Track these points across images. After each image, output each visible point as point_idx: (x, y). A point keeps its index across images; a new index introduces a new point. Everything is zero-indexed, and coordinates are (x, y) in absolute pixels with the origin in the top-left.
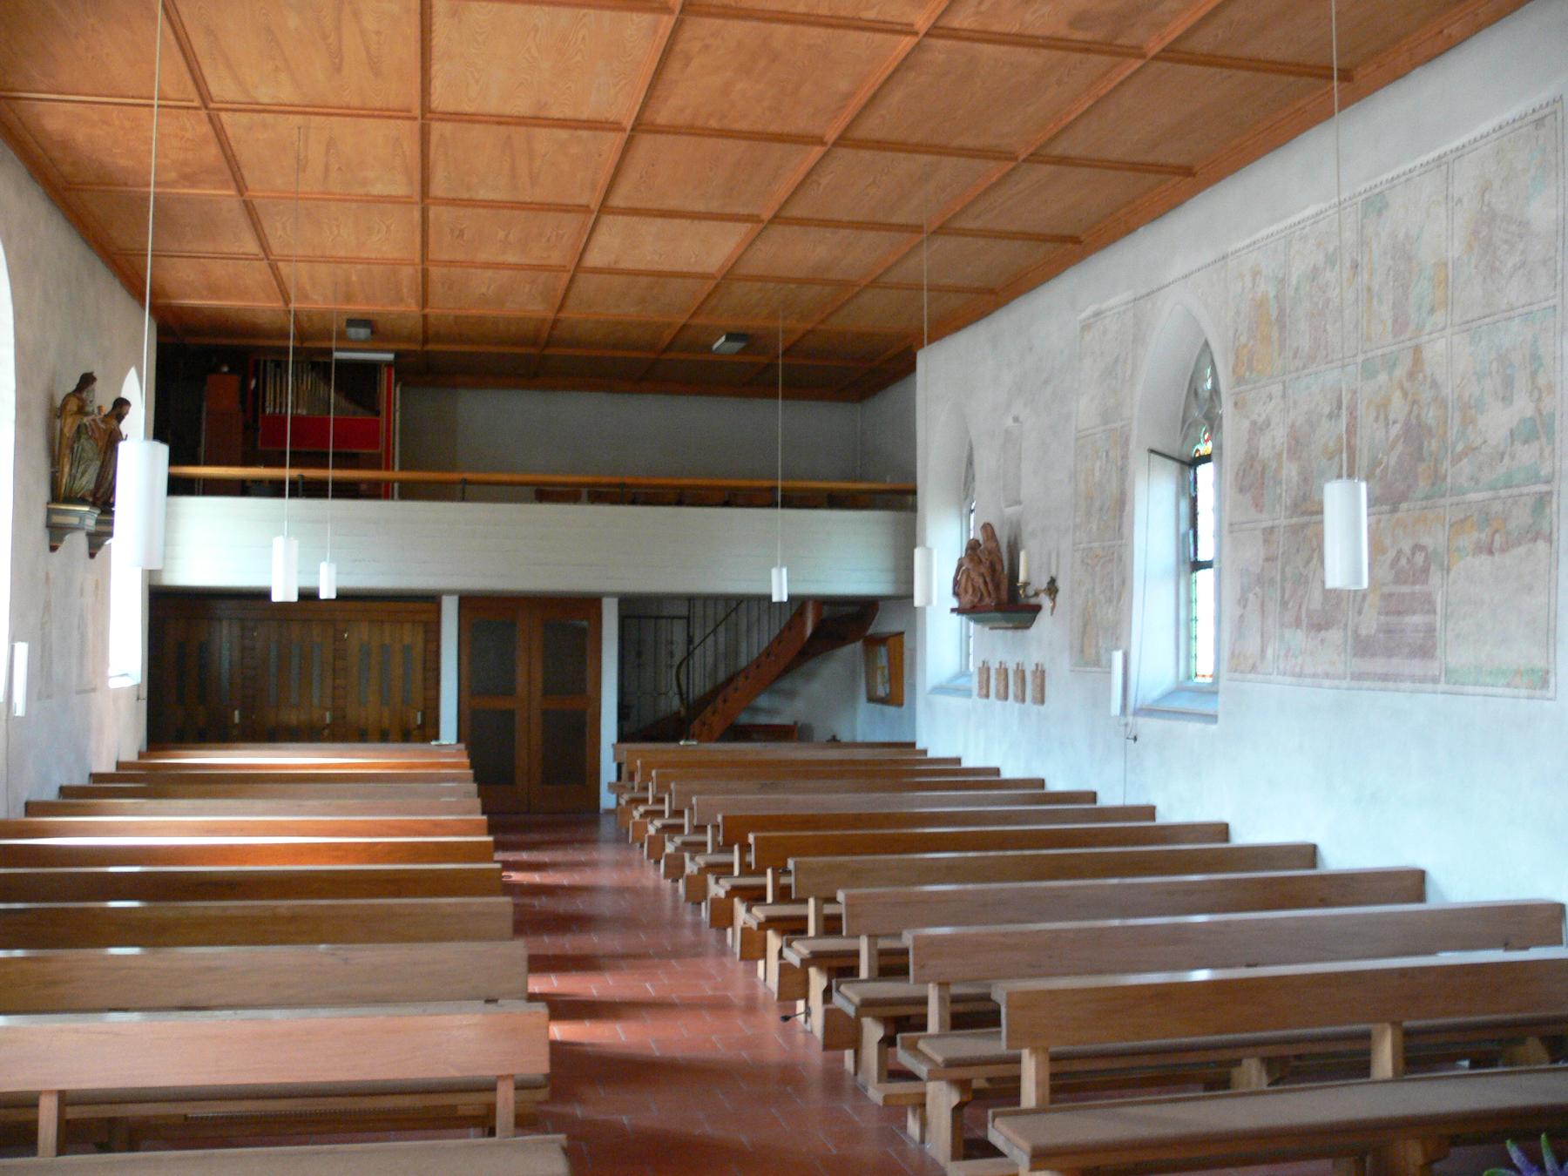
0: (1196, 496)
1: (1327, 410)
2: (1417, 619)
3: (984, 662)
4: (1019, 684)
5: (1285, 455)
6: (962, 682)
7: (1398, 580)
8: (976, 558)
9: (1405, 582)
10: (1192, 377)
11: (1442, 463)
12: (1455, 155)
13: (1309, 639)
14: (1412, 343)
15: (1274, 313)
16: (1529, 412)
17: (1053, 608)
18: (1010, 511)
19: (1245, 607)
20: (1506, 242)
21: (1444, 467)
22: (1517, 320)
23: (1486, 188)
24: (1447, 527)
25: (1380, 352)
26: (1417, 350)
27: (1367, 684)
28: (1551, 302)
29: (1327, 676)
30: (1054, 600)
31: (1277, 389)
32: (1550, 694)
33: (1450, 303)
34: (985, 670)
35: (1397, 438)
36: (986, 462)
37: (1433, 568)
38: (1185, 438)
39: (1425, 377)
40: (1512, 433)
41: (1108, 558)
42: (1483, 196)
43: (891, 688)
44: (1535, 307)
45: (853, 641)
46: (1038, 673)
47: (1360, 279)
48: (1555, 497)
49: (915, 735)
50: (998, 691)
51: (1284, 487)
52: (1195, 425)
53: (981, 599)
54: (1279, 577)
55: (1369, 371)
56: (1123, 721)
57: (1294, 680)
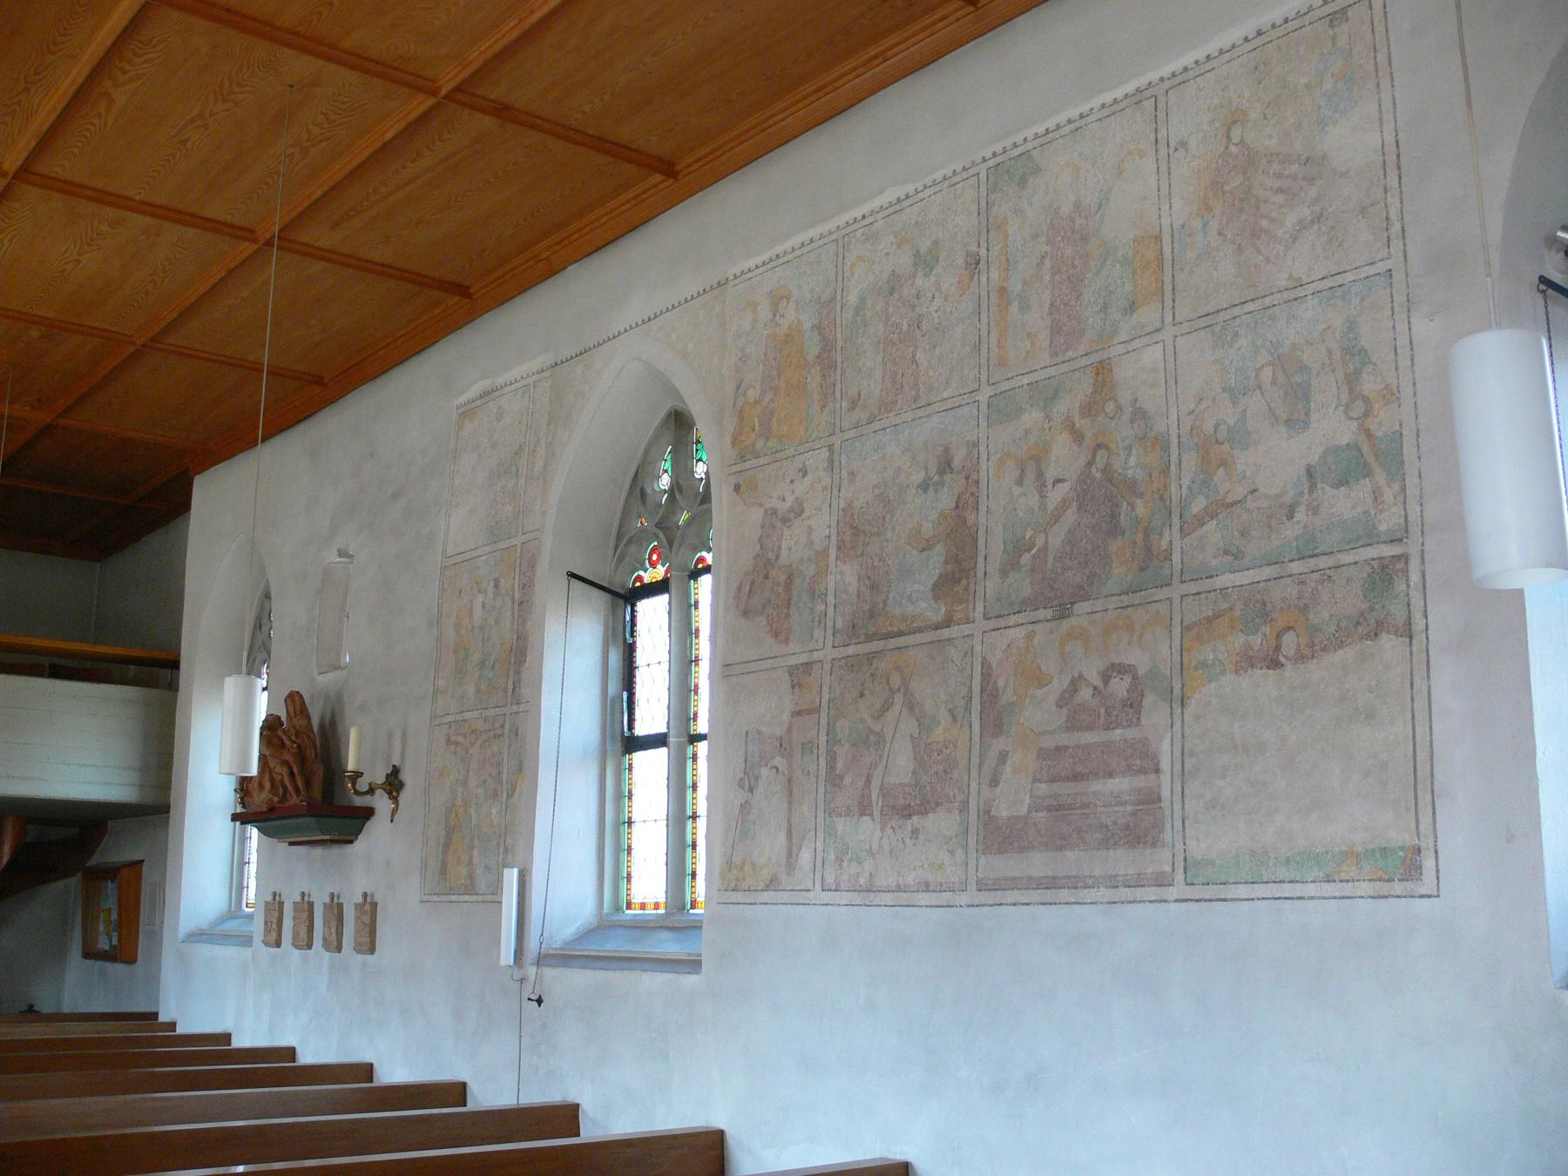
0: (634, 643)
1: (918, 477)
2: (1119, 785)
3: (275, 894)
4: (333, 923)
5: (833, 552)
6: (232, 925)
7: (1073, 725)
8: (276, 741)
9: (1090, 727)
10: (636, 475)
11: (1161, 534)
12: (1167, 84)
13: (889, 831)
14: (1095, 358)
15: (813, 348)
16: (1346, 434)
17: (394, 812)
18: (324, 680)
19: (751, 790)
20: (1280, 191)
21: (1166, 539)
22: (1312, 302)
23: (1235, 119)
24: (1177, 631)
25: (1025, 380)
26: (1103, 371)
27: (1011, 896)
28: (1381, 267)
29: (926, 887)
30: (395, 800)
31: (816, 460)
32: (1427, 884)
33: (1168, 289)
34: (274, 907)
35: (1064, 505)
36: (289, 616)
37: (1149, 699)
38: (620, 560)
39: (1119, 408)
40: (1310, 472)
41: (492, 734)
42: (1229, 129)
43: (120, 940)
44: (1350, 277)
45: (67, 875)
46: (367, 907)
47: (984, 279)
49: (156, 999)
50: (295, 937)
51: (831, 599)
52: (640, 538)
53: (284, 798)
54: (823, 738)
55: (1001, 410)
56: (518, 974)
57: (857, 898)
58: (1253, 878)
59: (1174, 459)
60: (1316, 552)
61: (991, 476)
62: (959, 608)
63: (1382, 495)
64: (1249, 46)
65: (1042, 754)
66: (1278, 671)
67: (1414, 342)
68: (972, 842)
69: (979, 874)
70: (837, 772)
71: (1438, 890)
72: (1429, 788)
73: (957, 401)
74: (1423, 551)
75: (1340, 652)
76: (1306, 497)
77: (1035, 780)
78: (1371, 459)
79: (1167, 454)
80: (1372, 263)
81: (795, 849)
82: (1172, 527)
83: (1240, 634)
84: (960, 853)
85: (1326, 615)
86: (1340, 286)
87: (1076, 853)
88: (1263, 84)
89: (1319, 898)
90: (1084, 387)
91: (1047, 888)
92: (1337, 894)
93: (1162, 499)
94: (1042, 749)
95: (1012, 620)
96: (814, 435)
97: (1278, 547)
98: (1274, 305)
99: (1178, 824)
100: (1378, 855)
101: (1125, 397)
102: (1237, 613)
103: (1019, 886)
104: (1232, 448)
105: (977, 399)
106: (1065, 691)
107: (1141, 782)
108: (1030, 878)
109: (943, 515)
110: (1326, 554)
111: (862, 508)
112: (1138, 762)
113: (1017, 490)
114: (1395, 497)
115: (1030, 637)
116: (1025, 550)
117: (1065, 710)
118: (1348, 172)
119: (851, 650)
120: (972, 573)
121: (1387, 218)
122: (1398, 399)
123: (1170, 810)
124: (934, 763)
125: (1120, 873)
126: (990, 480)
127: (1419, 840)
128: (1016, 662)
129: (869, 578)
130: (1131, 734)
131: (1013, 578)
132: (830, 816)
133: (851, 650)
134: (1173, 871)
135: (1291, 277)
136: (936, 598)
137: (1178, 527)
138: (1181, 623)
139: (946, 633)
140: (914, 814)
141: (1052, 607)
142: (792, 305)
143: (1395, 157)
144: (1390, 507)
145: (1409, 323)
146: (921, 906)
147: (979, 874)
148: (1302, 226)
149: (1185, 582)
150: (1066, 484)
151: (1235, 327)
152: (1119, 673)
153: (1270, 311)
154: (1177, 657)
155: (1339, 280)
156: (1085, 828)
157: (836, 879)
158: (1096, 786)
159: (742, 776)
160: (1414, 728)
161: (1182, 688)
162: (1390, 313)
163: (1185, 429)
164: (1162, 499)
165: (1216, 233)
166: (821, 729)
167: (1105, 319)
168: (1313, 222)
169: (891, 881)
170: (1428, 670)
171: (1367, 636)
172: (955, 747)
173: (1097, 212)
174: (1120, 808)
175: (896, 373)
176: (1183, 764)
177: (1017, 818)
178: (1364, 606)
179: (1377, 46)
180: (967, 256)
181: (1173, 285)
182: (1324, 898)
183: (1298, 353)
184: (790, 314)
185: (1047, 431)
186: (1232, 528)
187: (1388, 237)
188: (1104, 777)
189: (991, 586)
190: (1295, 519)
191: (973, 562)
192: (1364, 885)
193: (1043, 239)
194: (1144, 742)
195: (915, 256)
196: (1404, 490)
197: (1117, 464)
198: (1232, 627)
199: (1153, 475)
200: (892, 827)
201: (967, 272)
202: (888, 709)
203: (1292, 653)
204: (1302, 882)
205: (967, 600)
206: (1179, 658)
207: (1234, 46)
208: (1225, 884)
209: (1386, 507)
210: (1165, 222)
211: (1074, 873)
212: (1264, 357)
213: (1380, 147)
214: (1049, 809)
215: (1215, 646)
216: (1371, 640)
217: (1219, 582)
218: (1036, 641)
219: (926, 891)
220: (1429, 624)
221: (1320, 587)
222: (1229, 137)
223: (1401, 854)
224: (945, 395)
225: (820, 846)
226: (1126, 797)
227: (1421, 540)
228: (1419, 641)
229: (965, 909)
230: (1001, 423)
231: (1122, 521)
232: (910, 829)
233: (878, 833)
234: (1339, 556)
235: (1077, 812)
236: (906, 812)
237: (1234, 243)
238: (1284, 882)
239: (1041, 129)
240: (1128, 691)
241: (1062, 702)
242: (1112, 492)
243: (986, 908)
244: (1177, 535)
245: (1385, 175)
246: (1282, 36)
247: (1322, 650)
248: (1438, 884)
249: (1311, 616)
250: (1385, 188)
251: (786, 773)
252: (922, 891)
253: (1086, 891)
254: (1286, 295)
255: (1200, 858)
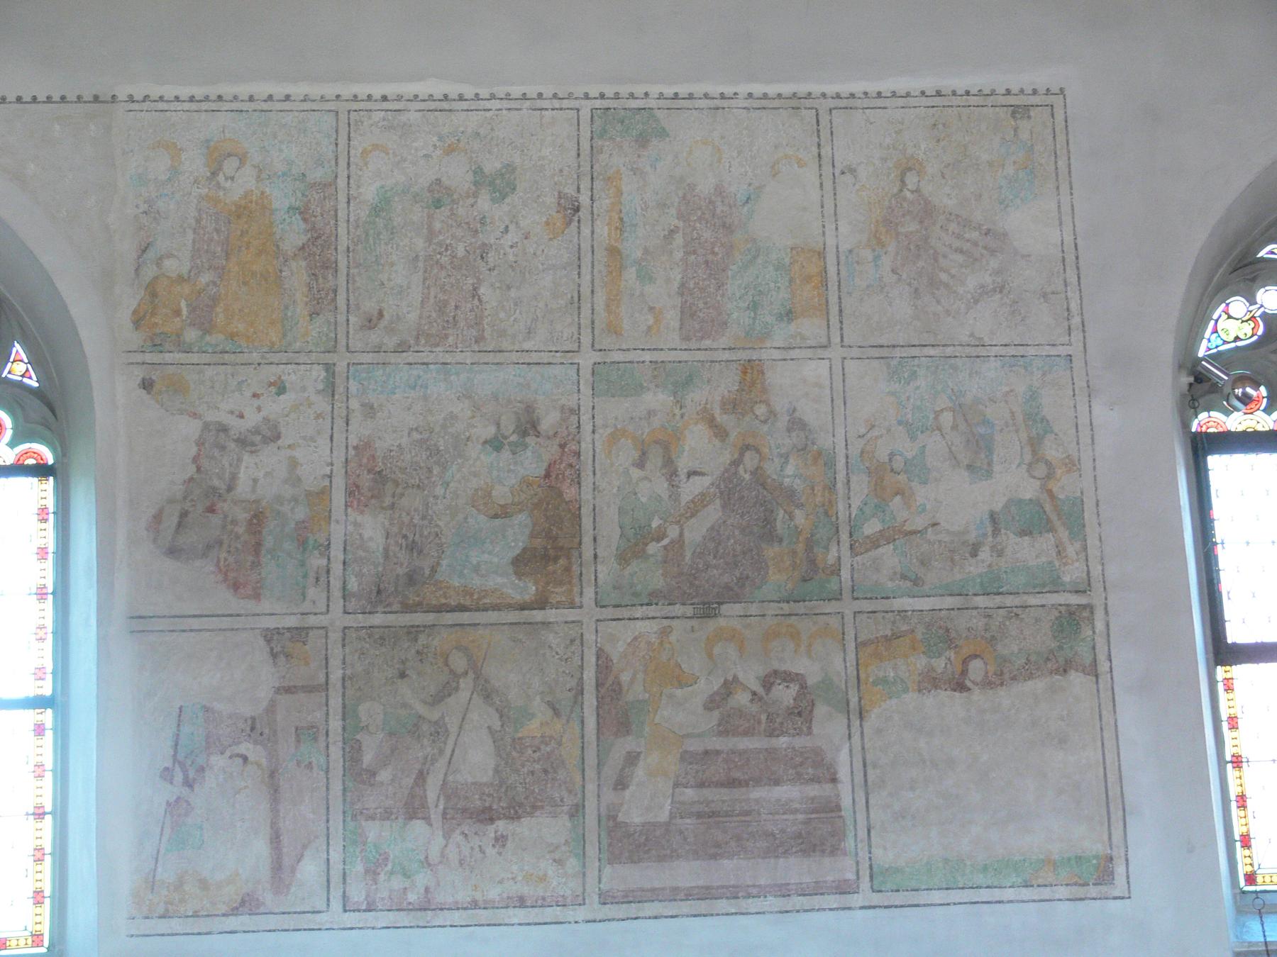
2: (788, 792)
5: (339, 498)
7: (725, 729)
11: (827, 548)
13: (457, 837)
15: (293, 235)
21: (833, 553)
22: (993, 363)
24: (851, 646)
26: (751, 373)
28: (1063, 351)
29: (521, 902)
32: (1119, 887)
33: (834, 310)
37: (821, 710)
39: (772, 413)
40: (993, 517)
44: (1031, 351)
47: (586, 231)
48: (1099, 615)
51: (337, 553)
58: (947, 884)
59: (841, 477)
60: (1001, 590)
61: (597, 450)
62: (556, 590)
63: (1065, 550)
64: (924, 101)
65: (687, 757)
66: (965, 694)
67: (1094, 424)
68: (592, 851)
69: (601, 886)
70: (364, 766)
71: (1129, 892)
72: (1121, 806)
73: (545, 357)
74: (1106, 604)
75: (1030, 683)
76: (990, 539)
77: (676, 785)
78: (1054, 517)
79: (833, 470)
80: (1054, 345)
81: (287, 861)
82: (841, 544)
83: (921, 655)
84: (572, 864)
85: (1016, 649)
86: (1022, 356)
87: (735, 861)
88: (942, 143)
89: (1018, 901)
90: (728, 383)
91: (698, 899)
92: (1035, 898)
93: (826, 513)
94: (686, 752)
95: (639, 612)
96: (298, 345)
97: (960, 580)
98: (956, 357)
99: (862, 833)
100: (1073, 862)
101: (780, 404)
102: (919, 636)
103: (660, 898)
104: (909, 480)
105: (576, 361)
106: (716, 693)
107: (813, 790)
108: (675, 890)
109: (526, 482)
110: (1011, 594)
111: (391, 451)
112: (810, 770)
113: (636, 473)
114: (1077, 553)
115: (665, 632)
116: (653, 540)
117: (716, 713)
118: (1029, 256)
119: (378, 619)
120: (576, 553)
121: (1068, 309)
122: (1079, 470)
123: (852, 820)
124: (528, 761)
125: (793, 881)
126: (597, 455)
127: (1111, 849)
128: (647, 657)
129: (405, 537)
130: (799, 742)
131: (635, 566)
132: (354, 817)
133: (378, 619)
134: (858, 878)
135: (972, 335)
136: (519, 575)
137: (848, 545)
138: (856, 638)
139: (538, 615)
140: (499, 819)
141: (692, 604)
142: (248, 171)
143: (1074, 258)
144: (1073, 561)
145: (1090, 407)
146: (513, 925)
147: (601, 886)
148: (984, 292)
149: (857, 599)
150: (705, 478)
151: (914, 366)
152: (784, 680)
153: (953, 361)
154: (852, 671)
155: (1021, 351)
156: (745, 836)
157: (367, 896)
158: (757, 793)
159: (169, 764)
160: (1104, 754)
161: (860, 701)
162: (1072, 393)
163: (855, 451)
164: (826, 513)
165: (890, 270)
166: (331, 711)
167: (754, 319)
168: (994, 290)
169: (463, 896)
170: (1114, 705)
171: (1057, 671)
172: (560, 744)
173: (744, 204)
174: (791, 817)
175: (445, 303)
176: (865, 775)
177: (655, 825)
178: (1053, 645)
179: (1058, 153)
180: (560, 197)
181: (840, 306)
182: (1023, 901)
183: (980, 406)
184: (241, 184)
185: (678, 417)
186: (911, 555)
187: (1069, 327)
188: (770, 785)
189: (605, 572)
190: (979, 558)
191: (577, 540)
192: (1062, 889)
193: (673, 211)
194: (818, 752)
195: (475, 173)
196: (1085, 548)
197: (771, 469)
198: (914, 649)
199: (816, 488)
200: (463, 833)
201: (560, 215)
202: (450, 695)
203: (979, 679)
204: (1000, 887)
205: (570, 583)
206: (855, 673)
207: (908, 95)
208: (917, 890)
209: (1070, 561)
210: (831, 242)
211: (732, 883)
212: (943, 402)
213: (1060, 243)
214: (699, 815)
215: (896, 664)
216: (1061, 675)
217: (898, 604)
218: (673, 638)
219: (520, 907)
220: (1113, 666)
221: (1008, 623)
222: (903, 181)
223: (1094, 862)
224: (526, 346)
225: (336, 856)
226: (798, 806)
227: (1104, 595)
228: (1104, 680)
229: (582, 926)
230: (613, 397)
231: (778, 527)
232: (492, 835)
233: (440, 840)
234: (1025, 597)
235: (735, 819)
236: (486, 816)
237: (910, 284)
238: (981, 887)
239: (669, 91)
240: (795, 699)
241: (712, 703)
242: (765, 496)
243: (615, 923)
244: (845, 553)
245: (1064, 270)
246: (963, 106)
247: (1012, 680)
248: (1129, 887)
249: (999, 647)
250: (1065, 281)
251: (264, 761)
252: (514, 907)
253: (750, 900)
254: (968, 350)
255: (887, 866)
